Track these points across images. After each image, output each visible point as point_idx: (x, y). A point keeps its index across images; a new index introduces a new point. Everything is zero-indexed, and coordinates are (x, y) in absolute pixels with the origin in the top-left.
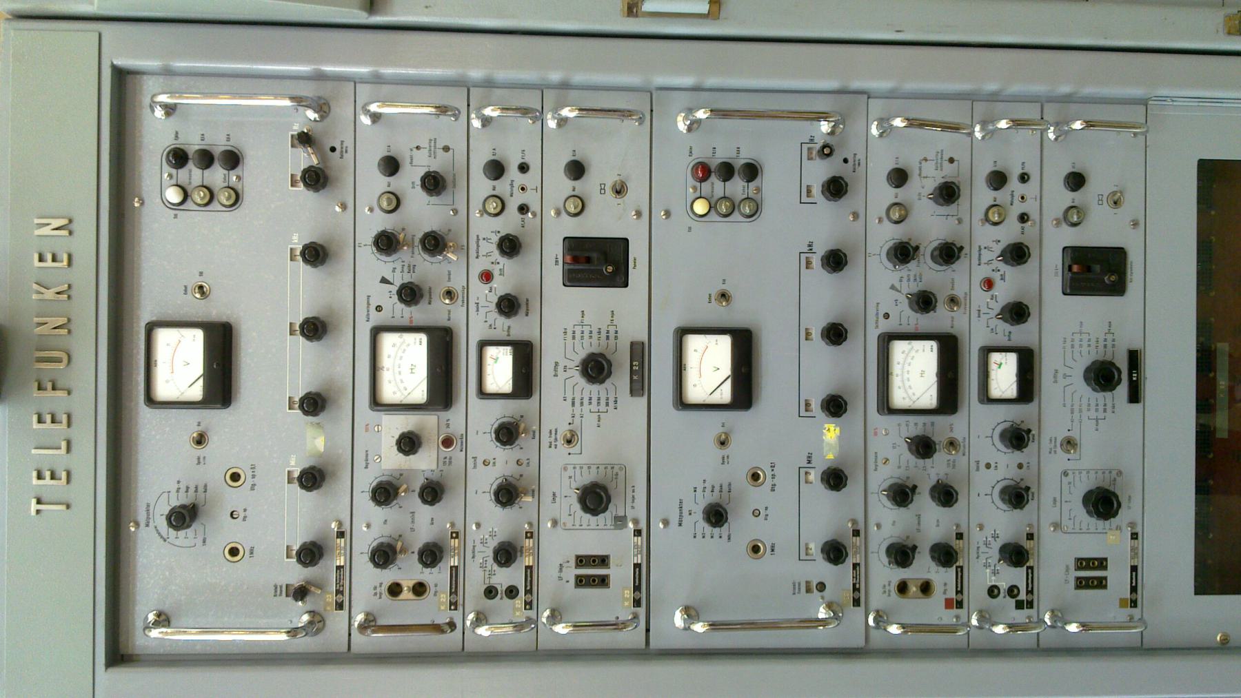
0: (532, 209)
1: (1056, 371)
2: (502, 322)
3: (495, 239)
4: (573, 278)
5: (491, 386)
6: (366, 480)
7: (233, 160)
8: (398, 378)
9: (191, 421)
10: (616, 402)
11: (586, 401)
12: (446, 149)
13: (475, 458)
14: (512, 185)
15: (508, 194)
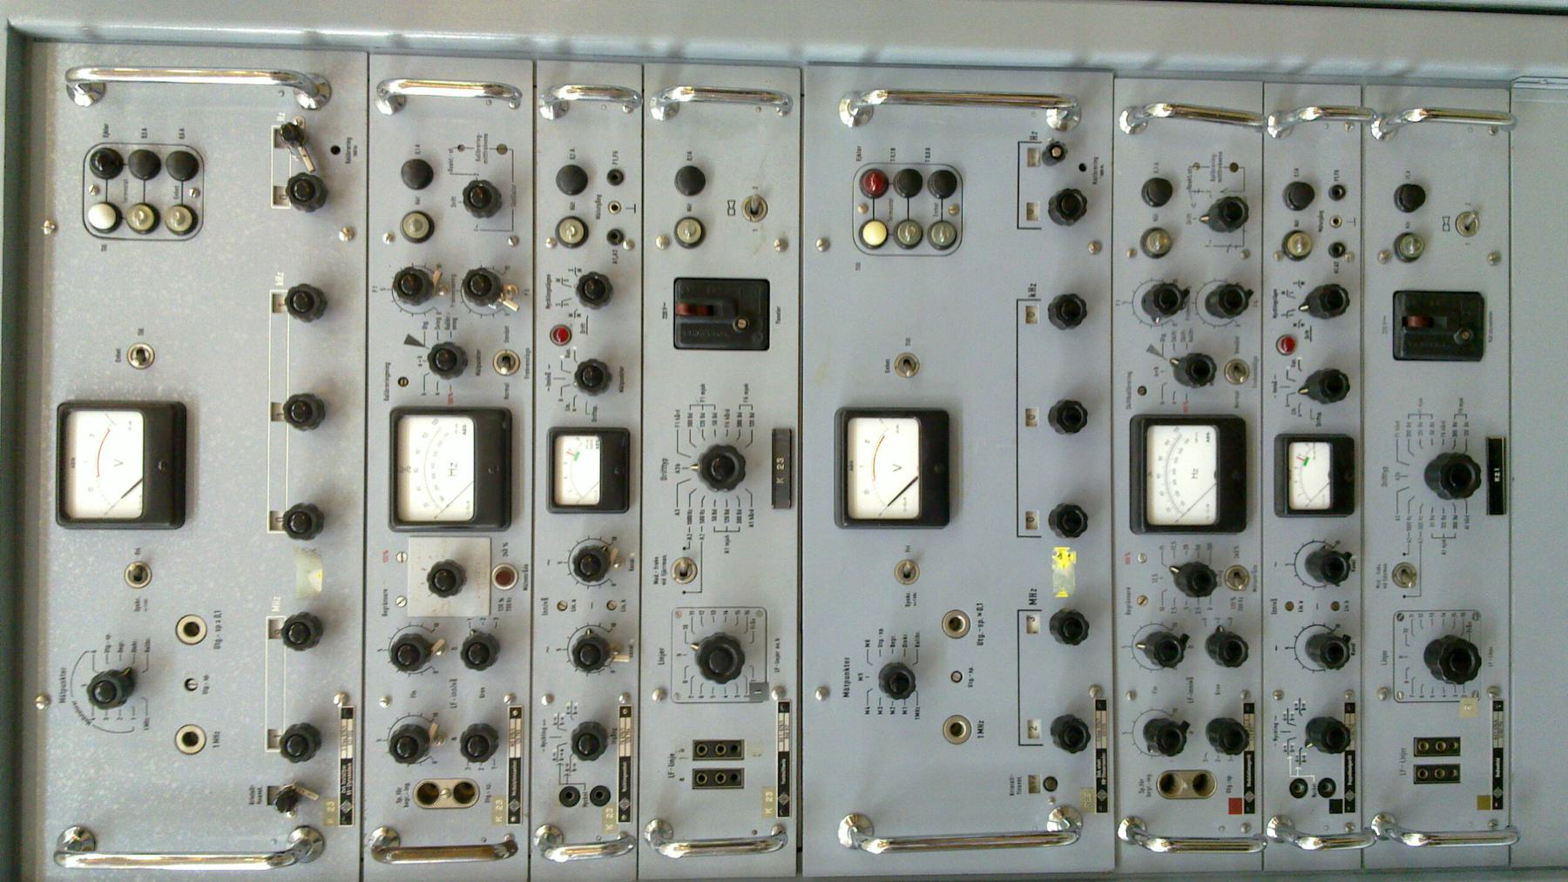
0: (628, 236)
1: (1386, 469)
2: (585, 401)
4: (688, 337)
5: (1300, 499)
6: (384, 634)
9: (124, 548)
10: (751, 517)
11: (708, 516)
12: (502, 149)
14: (598, 202)
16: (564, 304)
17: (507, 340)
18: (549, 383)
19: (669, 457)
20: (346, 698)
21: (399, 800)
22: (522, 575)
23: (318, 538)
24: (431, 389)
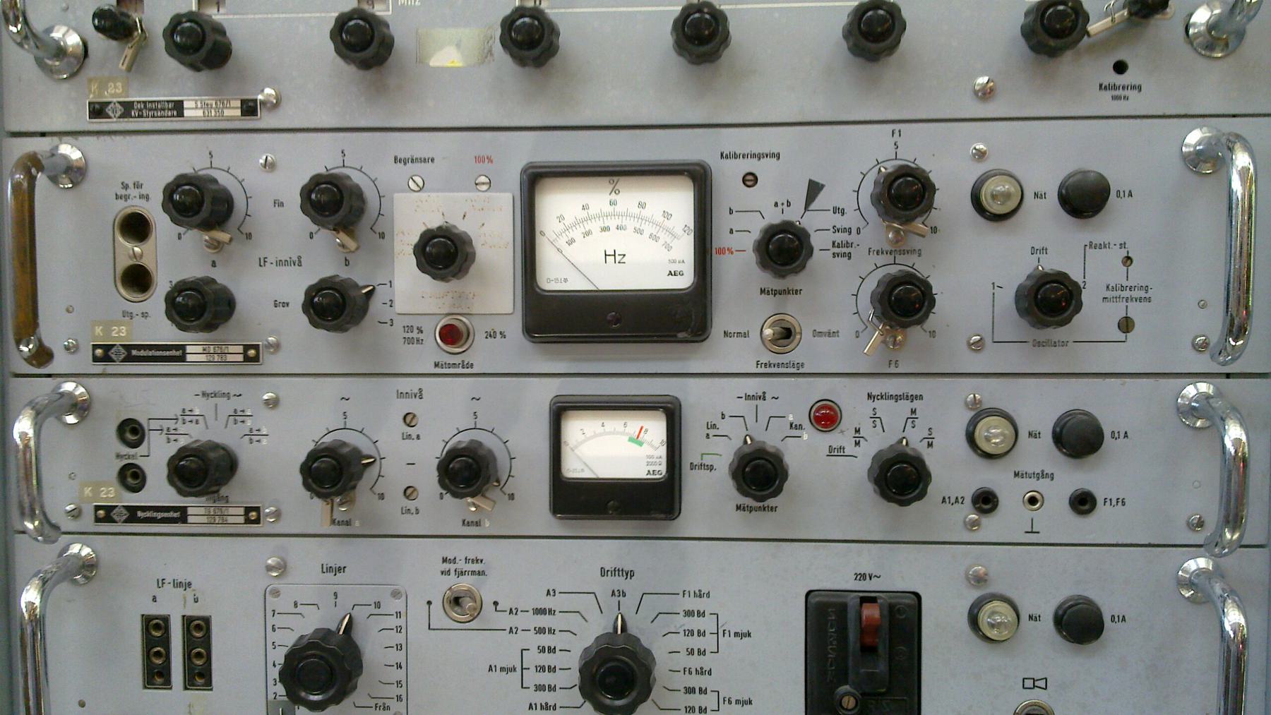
0: (986, 521)
1: (630, 574)
2: (723, 453)
3: (915, 441)
4: (826, 617)
5: (578, 429)
6: (366, 163)
8: (595, 226)
10: (546, 707)
11: (546, 640)
12: (1126, 325)
13: (420, 394)
14: (1042, 475)
15: (1021, 468)
17: (817, 334)
18: (748, 397)
20: (275, 105)
21: (126, 187)
22: (457, 360)
23: (507, 59)
24: (737, 221)
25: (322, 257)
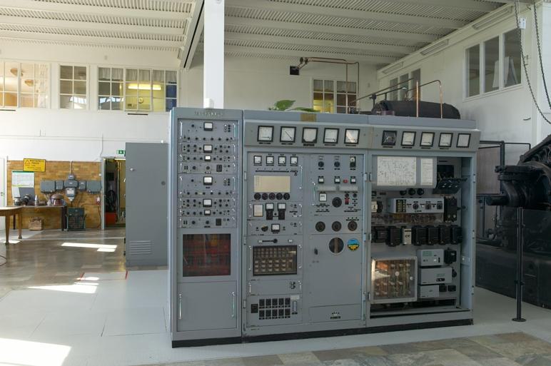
5: (206, 124)
7: (229, 131)
9: (202, 181)
16: (220, 157)
19: (209, 164)
25: (194, 203)
